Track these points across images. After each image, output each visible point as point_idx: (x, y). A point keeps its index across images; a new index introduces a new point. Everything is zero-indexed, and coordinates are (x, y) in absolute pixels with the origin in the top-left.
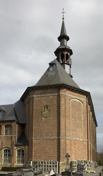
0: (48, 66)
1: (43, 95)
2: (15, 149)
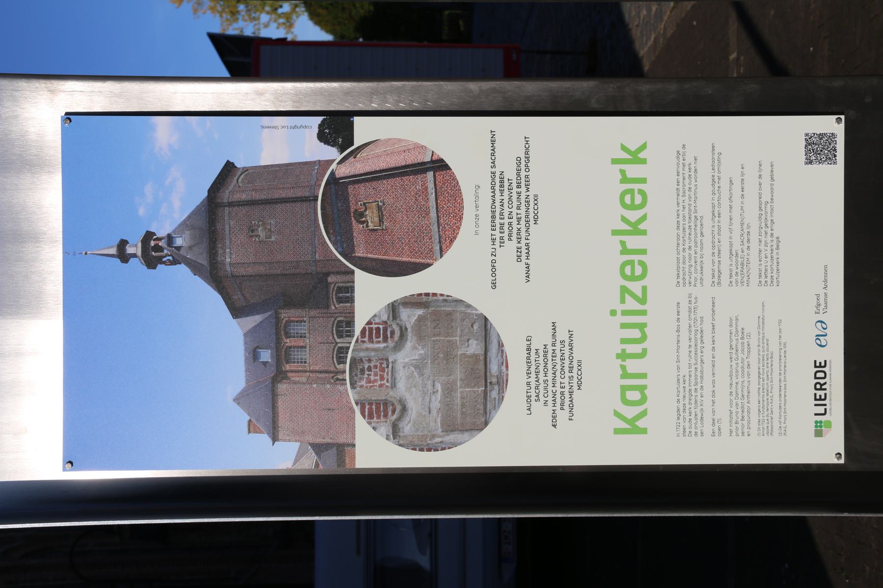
0: (160, 267)
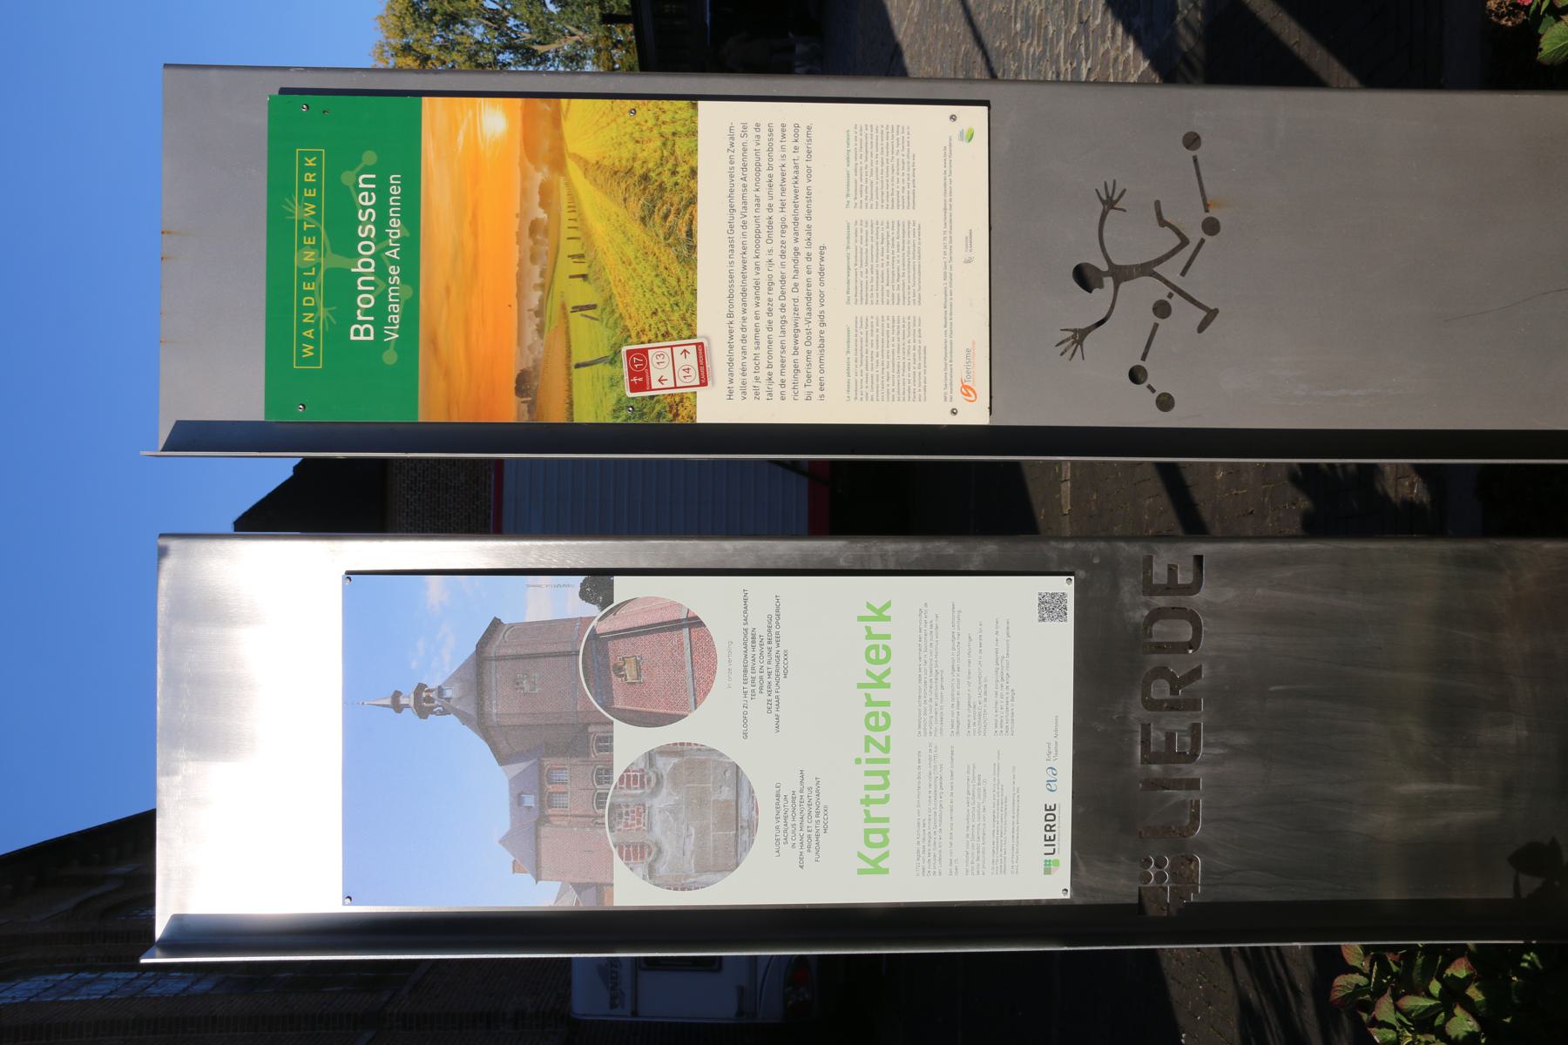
1: (494, 693)
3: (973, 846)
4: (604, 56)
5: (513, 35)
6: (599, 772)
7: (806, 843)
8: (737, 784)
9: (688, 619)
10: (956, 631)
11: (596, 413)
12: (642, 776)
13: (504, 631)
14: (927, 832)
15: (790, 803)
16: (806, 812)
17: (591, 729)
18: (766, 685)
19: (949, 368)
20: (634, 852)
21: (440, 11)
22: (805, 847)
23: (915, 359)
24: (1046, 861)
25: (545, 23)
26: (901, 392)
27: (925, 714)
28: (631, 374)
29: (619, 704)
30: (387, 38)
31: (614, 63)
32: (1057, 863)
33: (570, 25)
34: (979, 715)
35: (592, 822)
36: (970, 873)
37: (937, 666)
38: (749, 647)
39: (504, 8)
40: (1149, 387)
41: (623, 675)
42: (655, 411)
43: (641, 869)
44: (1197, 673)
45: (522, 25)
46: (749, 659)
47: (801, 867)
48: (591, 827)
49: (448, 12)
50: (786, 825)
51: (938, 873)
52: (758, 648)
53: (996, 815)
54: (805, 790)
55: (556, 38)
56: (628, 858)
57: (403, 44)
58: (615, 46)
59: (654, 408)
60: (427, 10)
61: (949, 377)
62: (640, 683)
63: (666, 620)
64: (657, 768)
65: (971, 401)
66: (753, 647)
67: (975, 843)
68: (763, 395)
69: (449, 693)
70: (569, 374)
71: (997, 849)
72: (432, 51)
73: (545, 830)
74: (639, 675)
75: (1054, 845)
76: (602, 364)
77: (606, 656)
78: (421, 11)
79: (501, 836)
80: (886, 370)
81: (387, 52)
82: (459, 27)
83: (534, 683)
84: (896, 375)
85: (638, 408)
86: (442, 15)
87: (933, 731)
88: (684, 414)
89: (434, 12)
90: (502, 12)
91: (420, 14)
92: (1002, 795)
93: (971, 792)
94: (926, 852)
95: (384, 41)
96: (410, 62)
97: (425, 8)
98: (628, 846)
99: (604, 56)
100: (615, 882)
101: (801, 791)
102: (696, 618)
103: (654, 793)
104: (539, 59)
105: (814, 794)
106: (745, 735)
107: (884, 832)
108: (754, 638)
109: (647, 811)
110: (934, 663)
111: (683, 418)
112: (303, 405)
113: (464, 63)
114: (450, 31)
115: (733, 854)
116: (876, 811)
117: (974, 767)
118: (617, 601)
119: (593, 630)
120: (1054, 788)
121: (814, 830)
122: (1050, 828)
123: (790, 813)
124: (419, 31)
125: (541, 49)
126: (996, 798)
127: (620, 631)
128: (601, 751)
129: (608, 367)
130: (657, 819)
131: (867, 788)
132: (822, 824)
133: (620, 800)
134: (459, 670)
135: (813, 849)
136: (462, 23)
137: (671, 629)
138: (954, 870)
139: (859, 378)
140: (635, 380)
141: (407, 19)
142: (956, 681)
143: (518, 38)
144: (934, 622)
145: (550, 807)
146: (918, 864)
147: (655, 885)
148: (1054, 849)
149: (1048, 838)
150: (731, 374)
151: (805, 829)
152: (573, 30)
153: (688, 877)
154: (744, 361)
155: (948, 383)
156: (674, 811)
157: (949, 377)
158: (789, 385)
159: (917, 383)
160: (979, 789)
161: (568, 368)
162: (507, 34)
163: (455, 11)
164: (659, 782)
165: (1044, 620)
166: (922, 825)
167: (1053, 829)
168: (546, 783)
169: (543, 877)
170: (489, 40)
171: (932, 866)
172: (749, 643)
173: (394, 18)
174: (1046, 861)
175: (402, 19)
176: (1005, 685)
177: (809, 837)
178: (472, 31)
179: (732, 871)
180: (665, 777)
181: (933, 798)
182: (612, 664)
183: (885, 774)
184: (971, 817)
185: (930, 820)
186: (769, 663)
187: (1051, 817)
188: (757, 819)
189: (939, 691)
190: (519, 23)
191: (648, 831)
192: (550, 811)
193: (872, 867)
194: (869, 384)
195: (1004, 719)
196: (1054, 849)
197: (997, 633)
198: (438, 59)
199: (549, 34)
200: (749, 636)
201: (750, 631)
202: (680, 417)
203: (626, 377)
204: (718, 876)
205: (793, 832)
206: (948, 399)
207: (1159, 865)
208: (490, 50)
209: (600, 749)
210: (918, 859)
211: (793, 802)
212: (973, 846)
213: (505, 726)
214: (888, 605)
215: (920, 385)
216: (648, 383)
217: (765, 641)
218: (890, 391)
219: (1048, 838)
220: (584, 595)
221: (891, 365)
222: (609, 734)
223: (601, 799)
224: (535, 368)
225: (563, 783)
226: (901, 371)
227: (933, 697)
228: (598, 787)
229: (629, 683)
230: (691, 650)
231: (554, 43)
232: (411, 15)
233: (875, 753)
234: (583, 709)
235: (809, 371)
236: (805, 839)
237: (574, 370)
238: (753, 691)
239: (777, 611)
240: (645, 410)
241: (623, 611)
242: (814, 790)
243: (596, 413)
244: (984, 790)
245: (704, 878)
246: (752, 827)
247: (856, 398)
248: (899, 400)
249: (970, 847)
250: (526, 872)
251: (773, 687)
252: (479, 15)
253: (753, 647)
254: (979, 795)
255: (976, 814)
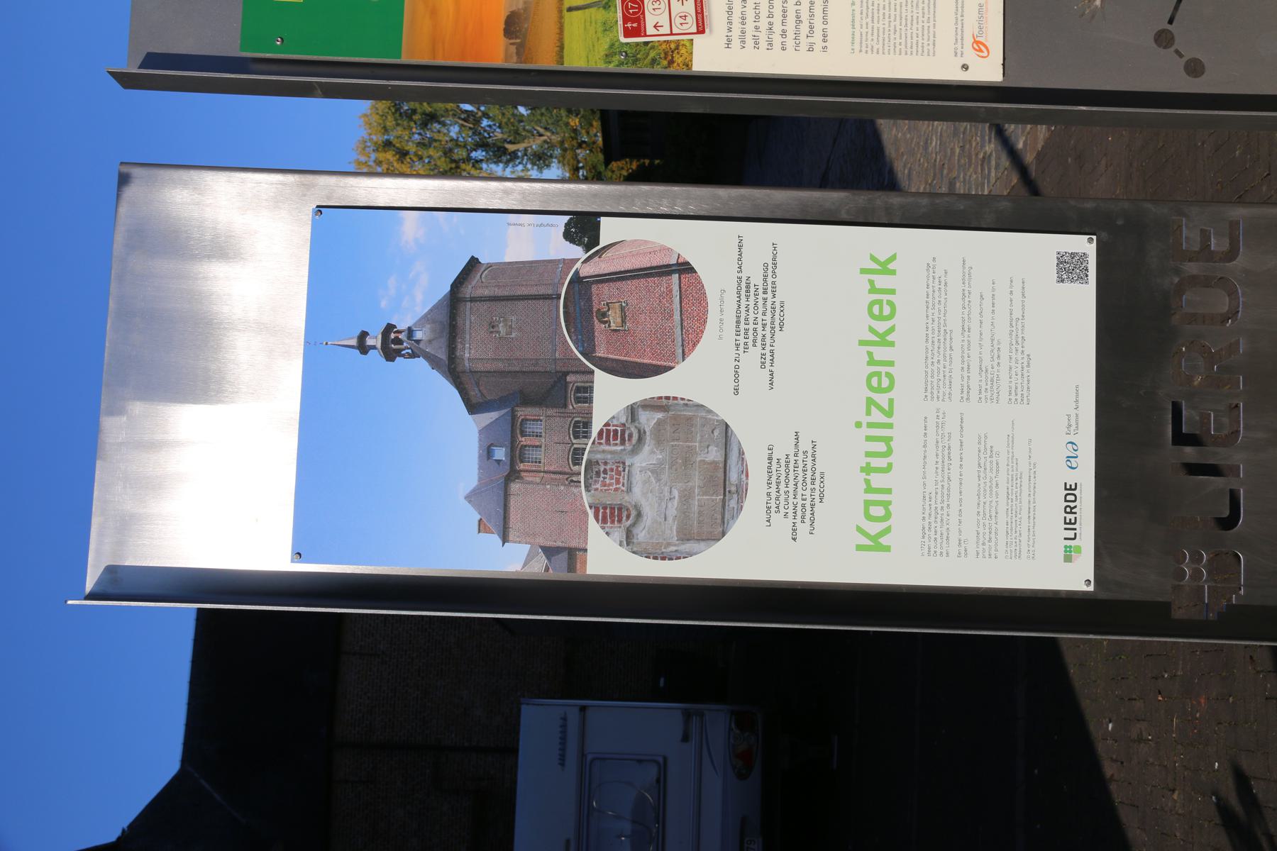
1: (468, 337)
2: (574, 408)
3: (984, 525)
4: (569, 155)
5: (486, 134)
6: (576, 424)
7: (799, 513)
8: (726, 444)
9: (678, 264)
10: (967, 289)
11: (588, 57)
12: (623, 432)
13: (482, 270)
14: (933, 507)
15: (783, 468)
16: (800, 478)
17: (569, 378)
18: (759, 338)
19: (960, 22)
20: (611, 514)
21: (419, 111)
22: (799, 517)
23: (924, 13)
24: (1066, 547)
25: (516, 124)
26: (909, 45)
27: (932, 377)
28: (626, 20)
29: (601, 352)
30: (370, 134)
31: (579, 162)
32: (1078, 549)
33: (538, 126)
34: (992, 380)
35: (567, 479)
36: (981, 555)
37: (945, 325)
38: (743, 297)
39: (478, 109)
40: (1177, 52)
41: (606, 322)
42: (650, 57)
43: (619, 534)
44: (1233, 348)
45: (495, 125)
46: (743, 309)
47: (794, 539)
48: (565, 485)
49: (427, 112)
50: (778, 492)
51: (945, 554)
52: (752, 298)
53: (1010, 492)
54: (800, 454)
55: (525, 138)
56: (604, 521)
57: (384, 140)
58: (580, 146)
59: (648, 54)
60: (408, 110)
61: (959, 32)
62: (625, 330)
63: (655, 264)
64: (639, 423)
65: (982, 57)
66: (748, 297)
67: (987, 522)
68: (763, 44)
69: (419, 335)
70: (561, 17)
71: (1012, 529)
72: (411, 147)
73: (515, 487)
74: (623, 322)
75: (1075, 529)
76: (596, 8)
77: (589, 300)
78: (402, 111)
79: (468, 491)
80: (892, 24)
81: (369, 147)
82: (436, 126)
83: (511, 327)
84: (904, 29)
85: (633, 55)
86: (421, 115)
87: (941, 394)
88: (679, 62)
89: (414, 111)
90: (477, 113)
91: (401, 114)
92: (1017, 470)
93: (982, 465)
94: (933, 530)
95: (366, 137)
96: (389, 155)
97: (406, 108)
98: (605, 508)
99: (569, 155)
100: (589, 547)
101: (796, 455)
102: (688, 263)
103: (635, 451)
104: (509, 157)
105: (810, 458)
106: (736, 391)
107: (886, 504)
108: (748, 287)
109: (627, 470)
110: (942, 322)
111: (678, 65)
112: (282, 39)
113: (439, 158)
114: (428, 129)
115: (719, 521)
116: (877, 480)
117: (986, 437)
118: (603, 243)
119: (577, 272)
120: (1074, 466)
121: (809, 499)
122: (1070, 510)
123: (782, 478)
124: (399, 128)
125: (511, 148)
126: (1010, 473)
127: (605, 275)
128: (579, 402)
129: (602, 11)
130: (638, 478)
131: (868, 454)
132: (817, 493)
133: (599, 456)
134: (431, 310)
135: (807, 520)
136: (439, 123)
137: (660, 275)
138: (963, 552)
139: (864, 30)
140: (629, 25)
141: (389, 117)
142: (966, 343)
143: (490, 137)
144: (943, 279)
145: (522, 462)
146: (923, 544)
147: (634, 552)
148: (1075, 534)
149: (1068, 521)
150: (730, 23)
151: (799, 496)
152: (542, 131)
153: (669, 544)
154: (744, 10)
155: (959, 38)
156: (656, 471)
157: (959, 32)
158: (790, 35)
159: (926, 37)
160: (991, 462)
161: (560, 11)
162: (480, 133)
163: (433, 111)
164: (641, 439)
165: (1062, 281)
166: (927, 498)
167: (1073, 511)
168: (519, 436)
169: (511, 538)
170: (464, 138)
171: (939, 546)
172: (743, 293)
173: (378, 117)
174: (1066, 547)
175: (384, 118)
176: (1020, 349)
177: (803, 506)
178: (448, 130)
179: (719, 540)
180: (648, 433)
181: (940, 469)
182: (595, 310)
183: (888, 440)
184: (982, 492)
185: (936, 493)
186: (764, 314)
187: (1072, 498)
188: (747, 484)
189: (948, 352)
190: (492, 123)
191: (627, 492)
192: (522, 466)
193: (872, 544)
194: (875, 37)
195: (1019, 386)
196: (1075, 534)
197: (1011, 292)
198: (416, 154)
199: (519, 134)
200: (743, 285)
201: (744, 280)
202: (675, 64)
203: (620, 22)
204: (702, 544)
205: (786, 500)
206: (959, 54)
207: (1197, 558)
208: (465, 146)
209: (578, 400)
210: (923, 537)
211: (787, 466)
212: (984, 525)
213: (477, 372)
214: (893, 258)
215: (929, 40)
216: (643, 28)
217: (761, 291)
218: (897, 45)
219: (1068, 521)
220: (568, 236)
221: (898, 18)
222: (590, 384)
223: (577, 455)
224: (525, 10)
225: (537, 436)
226: (909, 25)
227: (941, 358)
228: (574, 441)
229: (614, 330)
230: (680, 297)
231: (524, 142)
232: (393, 114)
233: (877, 417)
234: (561, 357)
235: (812, 21)
236: (799, 508)
237: (567, 15)
238: (746, 344)
239: (774, 259)
240: (639, 56)
241: (609, 254)
242: (809, 454)
243: (588, 57)
244: (997, 464)
245: (687, 547)
246: (741, 492)
247: (861, 51)
248: (906, 54)
249: (981, 526)
250: (493, 533)
251: (768, 341)
252: (455, 115)
253: (748, 297)
254: (991, 469)
255: (988, 489)
